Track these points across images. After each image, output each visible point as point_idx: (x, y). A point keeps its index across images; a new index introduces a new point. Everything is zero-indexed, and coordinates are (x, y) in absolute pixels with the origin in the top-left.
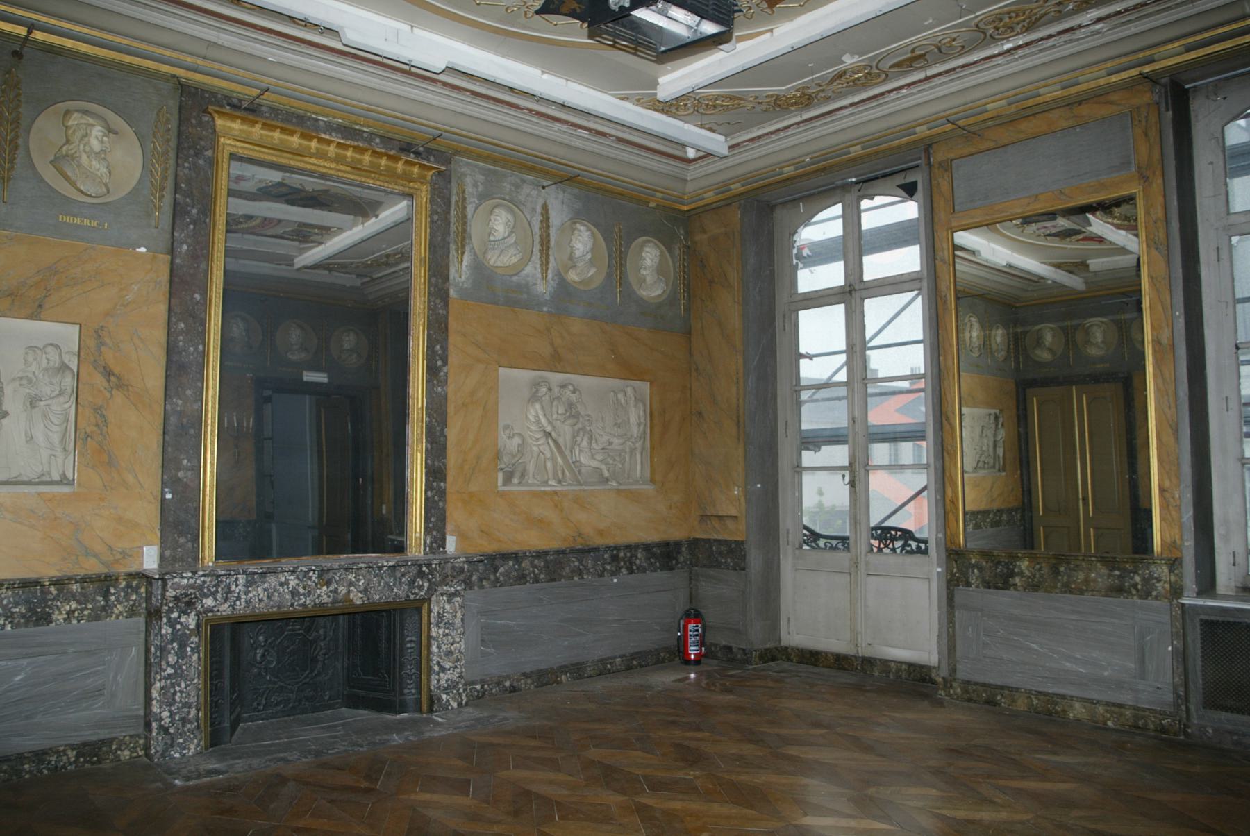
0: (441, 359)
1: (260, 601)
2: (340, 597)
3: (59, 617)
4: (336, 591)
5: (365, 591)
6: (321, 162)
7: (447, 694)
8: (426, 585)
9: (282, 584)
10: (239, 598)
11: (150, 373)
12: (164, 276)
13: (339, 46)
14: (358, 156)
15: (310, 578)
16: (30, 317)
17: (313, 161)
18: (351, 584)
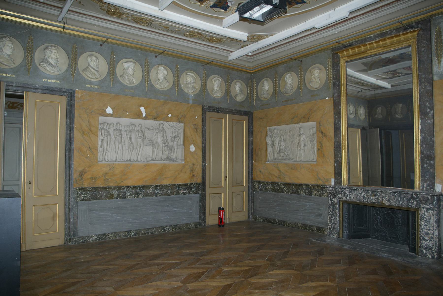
0: (429, 108)
1: (354, 198)
2: (379, 201)
3: (314, 194)
4: (378, 199)
5: (389, 201)
6: (373, 51)
7: (426, 250)
8: (415, 203)
9: (360, 194)
10: (348, 196)
11: (331, 132)
12: (333, 104)
13: (317, 30)
14: (384, 42)
15: (369, 193)
16: (307, 122)
17: (370, 52)
18: (383, 197)
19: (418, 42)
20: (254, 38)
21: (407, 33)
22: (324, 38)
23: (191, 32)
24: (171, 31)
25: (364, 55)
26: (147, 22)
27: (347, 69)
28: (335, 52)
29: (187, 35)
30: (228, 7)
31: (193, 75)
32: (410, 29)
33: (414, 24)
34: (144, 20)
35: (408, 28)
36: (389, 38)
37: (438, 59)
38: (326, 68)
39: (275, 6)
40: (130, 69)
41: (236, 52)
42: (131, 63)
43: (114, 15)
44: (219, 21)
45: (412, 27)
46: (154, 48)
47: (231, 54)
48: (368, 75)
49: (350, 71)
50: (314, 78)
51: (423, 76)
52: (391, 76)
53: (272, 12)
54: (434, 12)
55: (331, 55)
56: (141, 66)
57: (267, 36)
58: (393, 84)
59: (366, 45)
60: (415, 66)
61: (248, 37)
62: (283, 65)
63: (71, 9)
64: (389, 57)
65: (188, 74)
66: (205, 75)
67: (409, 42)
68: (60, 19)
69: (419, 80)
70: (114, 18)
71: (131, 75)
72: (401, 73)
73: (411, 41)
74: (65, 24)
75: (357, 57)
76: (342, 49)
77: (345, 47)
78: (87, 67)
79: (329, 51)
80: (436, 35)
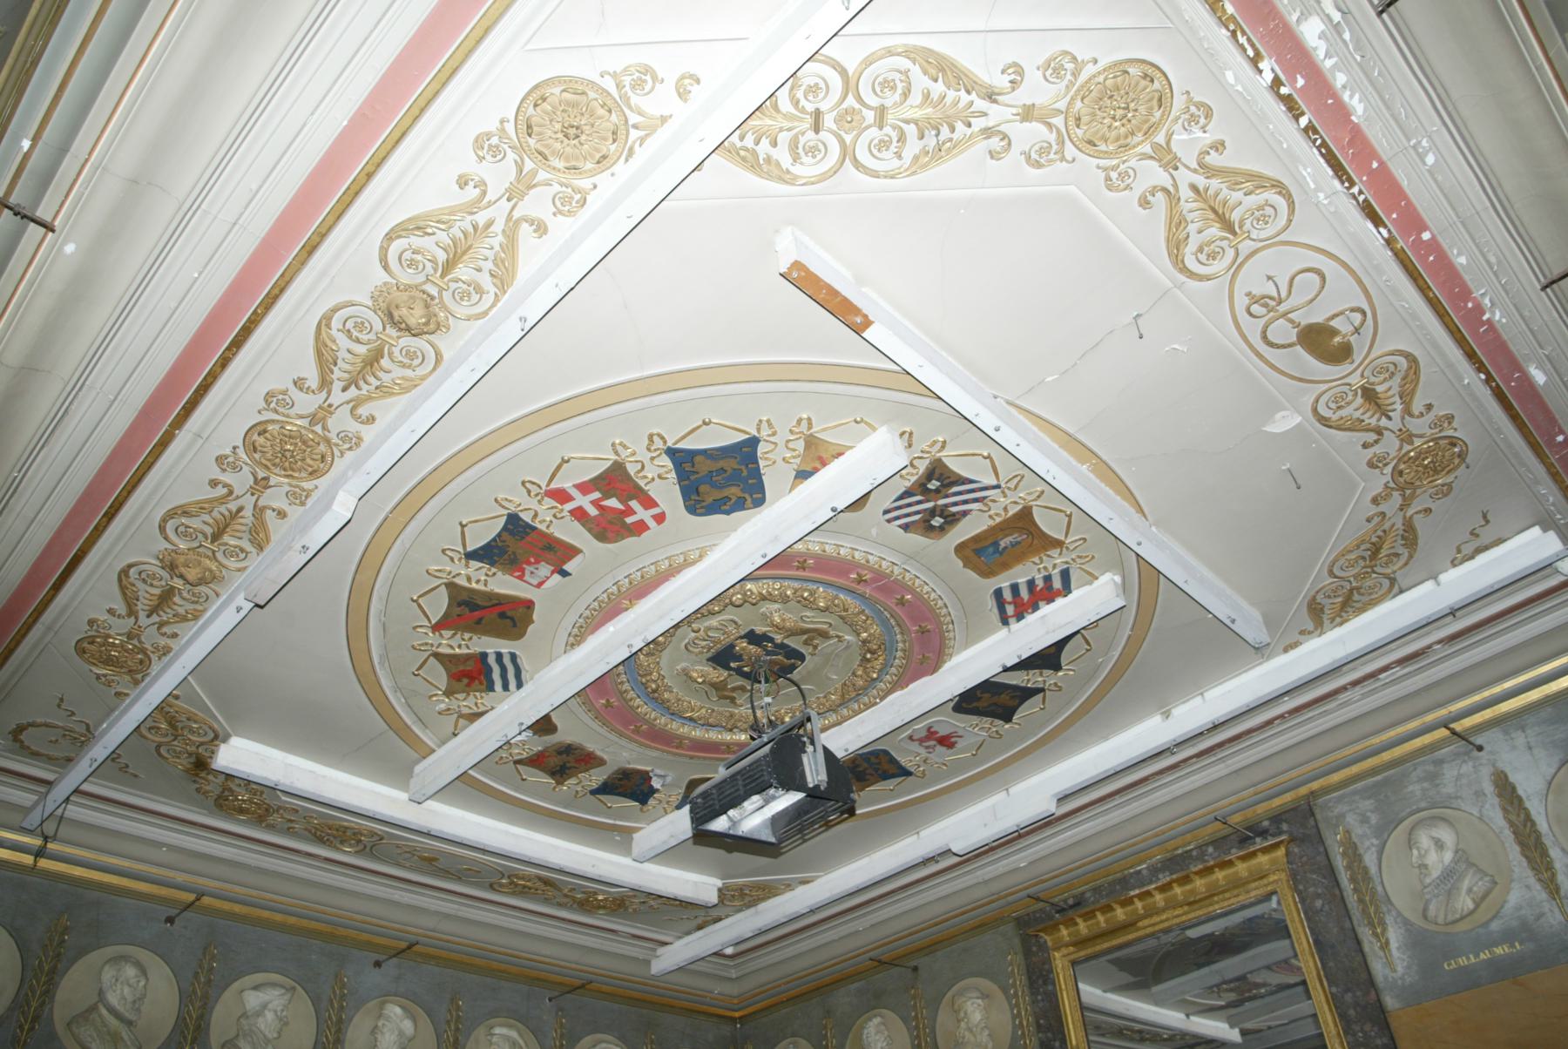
6: (1156, 919)
13: (957, 859)
14: (1188, 887)
17: (1146, 922)
19: (1295, 878)
20: (743, 895)
21: (1253, 854)
22: (986, 882)
23: (517, 876)
24: (445, 873)
25: (1130, 937)
26: (359, 841)
27: (1081, 985)
28: (1031, 931)
29: (501, 885)
30: (653, 791)
31: (514, 1034)
32: (1258, 840)
33: (1266, 823)
34: (349, 833)
35: (1249, 838)
36: (1200, 873)
37: (1375, 934)
38: (1005, 990)
39: (814, 794)
40: (269, 1015)
41: (679, 944)
42: (277, 992)
43: (241, 811)
44: (619, 838)
45: (1263, 833)
46: (378, 934)
47: (661, 951)
48: (1157, 1002)
49: (1092, 993)
50: (970, 1030)
51: (1348, 997)
52: (1232, 996)
53: (807, 812)
54: (1315, 785)
55: (1017, 941)
56: (316, 1001)
57: (789, 887)
58: (1249, 1025)
59: (1130, 901)
60: (1311, 964)
61: (720, 890)
62: (856, 985)
63: (86, 787)
64: (1212, 934)
65: (497, 1030)
66: (562, 1036)
67: (1265, 881)
68: (34, 819)
69: (1340, 1015)
70: (240, 822)
71: (268, 1041)
72: (1264, 985)
73: (1272, 878)
74: (46, 839)
75: (1106, 945)
76: (1051, 918)
77: (1061, 911)
78: (93, 1008)
79: (1009, 928)
80: (1344, 854)
